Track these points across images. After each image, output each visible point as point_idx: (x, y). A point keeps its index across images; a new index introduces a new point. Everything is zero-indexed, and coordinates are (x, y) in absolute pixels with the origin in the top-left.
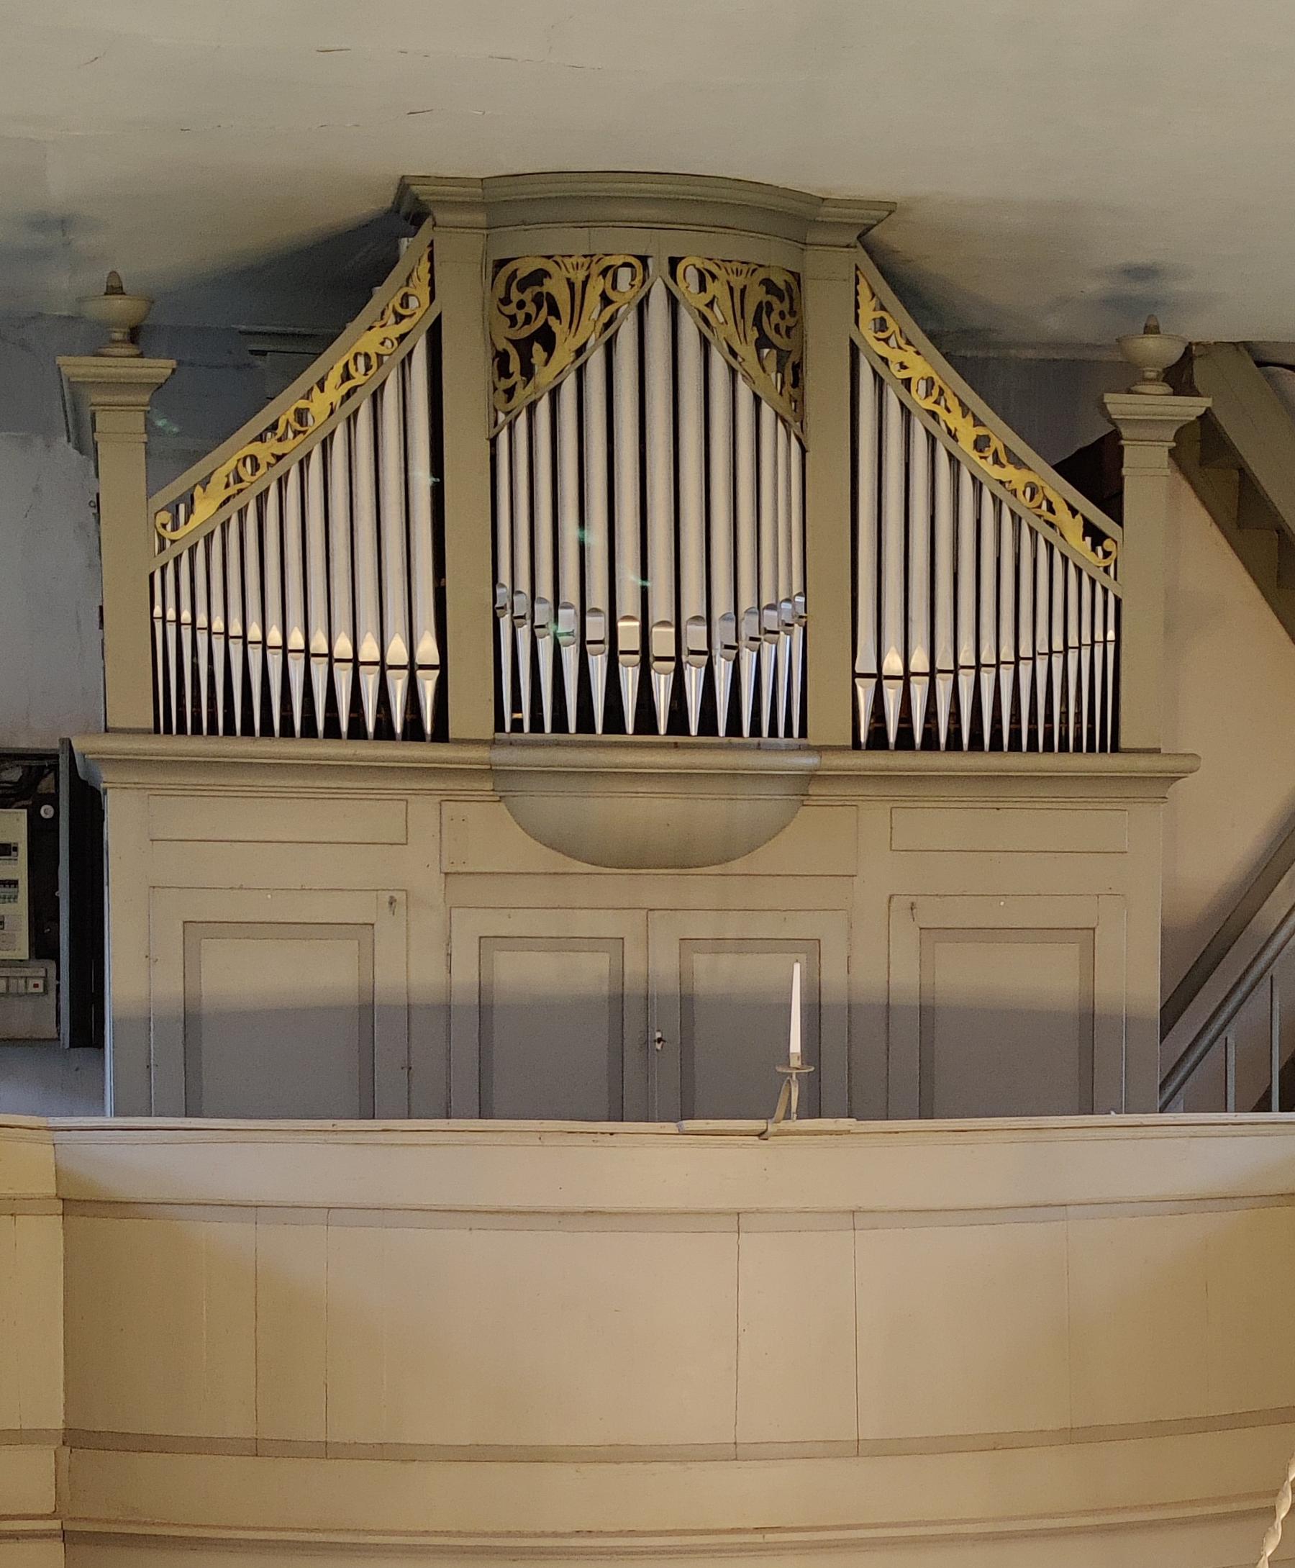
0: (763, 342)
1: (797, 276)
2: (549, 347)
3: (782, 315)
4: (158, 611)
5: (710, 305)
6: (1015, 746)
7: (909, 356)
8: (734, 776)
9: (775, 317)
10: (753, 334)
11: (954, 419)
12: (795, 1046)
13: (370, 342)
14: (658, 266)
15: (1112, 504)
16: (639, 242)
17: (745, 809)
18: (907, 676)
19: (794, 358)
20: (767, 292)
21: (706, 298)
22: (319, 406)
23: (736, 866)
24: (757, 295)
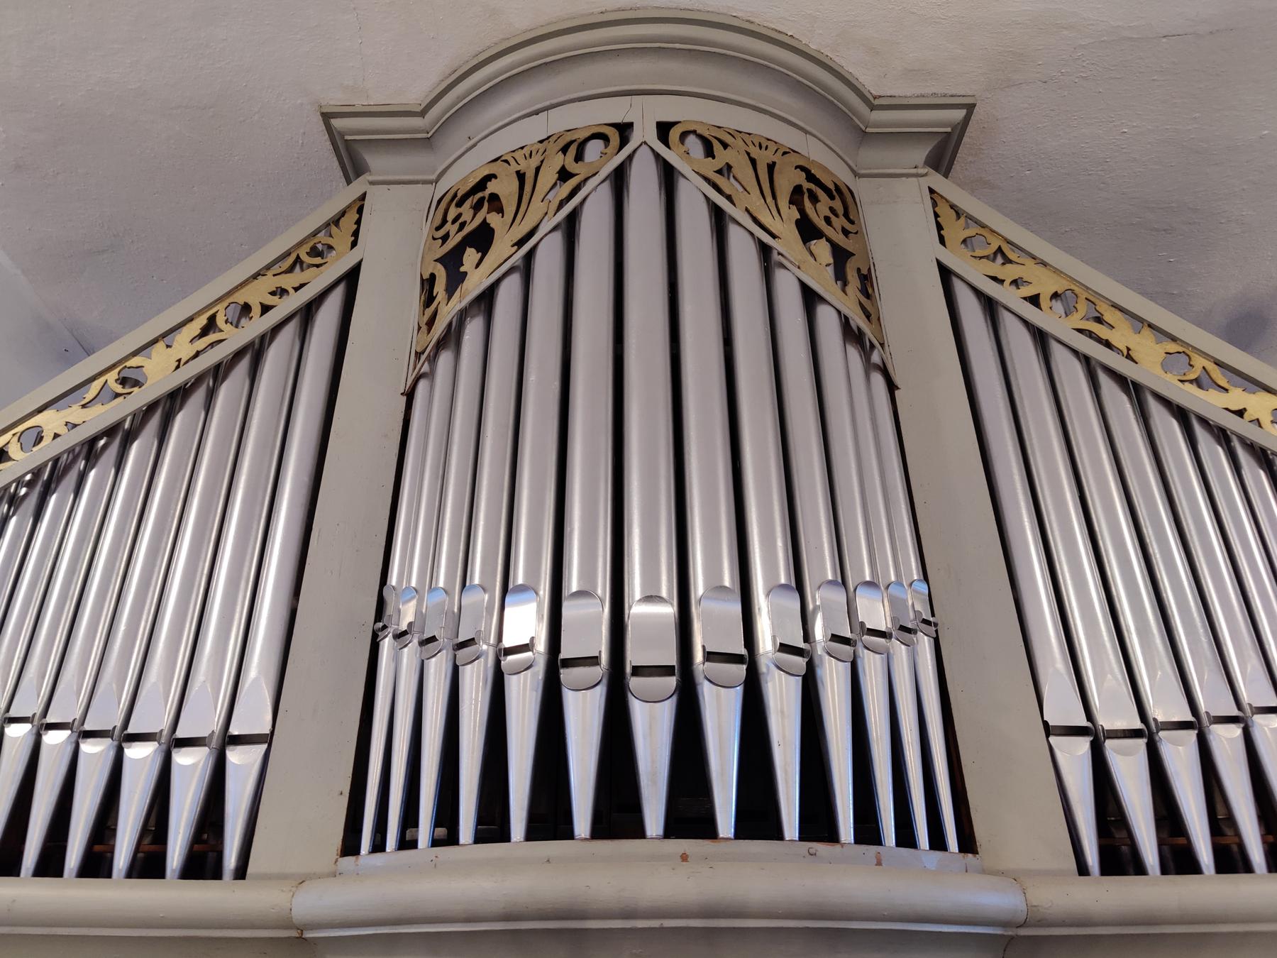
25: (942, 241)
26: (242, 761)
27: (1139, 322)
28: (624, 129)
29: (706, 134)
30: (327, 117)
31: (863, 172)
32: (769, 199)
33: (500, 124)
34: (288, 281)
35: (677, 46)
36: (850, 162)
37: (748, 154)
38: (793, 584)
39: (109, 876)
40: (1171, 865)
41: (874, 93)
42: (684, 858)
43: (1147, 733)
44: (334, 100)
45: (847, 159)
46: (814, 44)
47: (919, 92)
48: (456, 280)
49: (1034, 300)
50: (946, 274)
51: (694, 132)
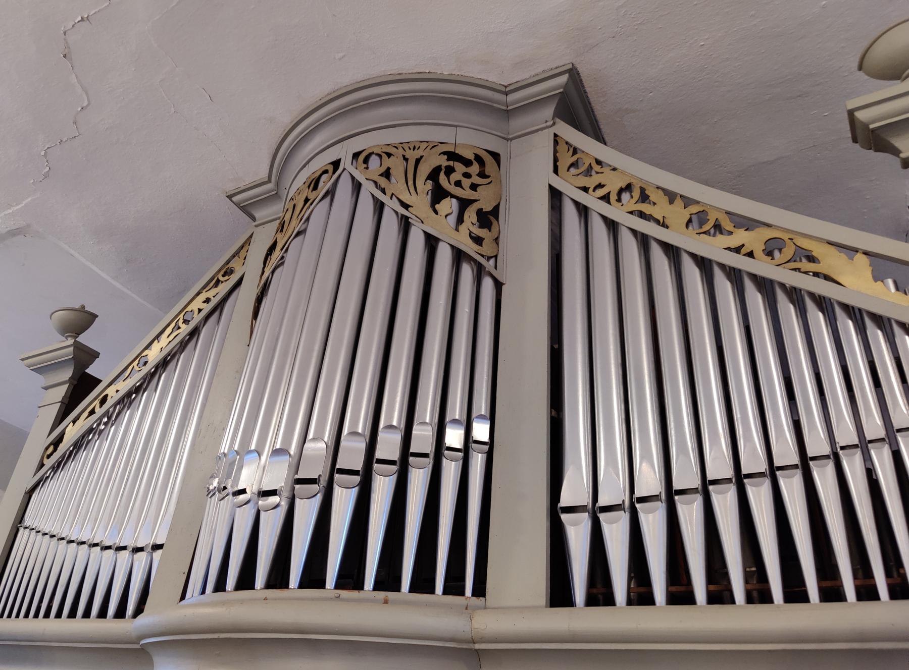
0: (439, 195)
1: (496, 156)
3: (467, 175)
4: (574, 491)
5: (387, 174)
9: (455, 177)
20: (448, 160)
21: (383, 169)
25: (556, 171)
27: (671, 197)
28: (336, 164)
29: (379, 152)
30: (230, 197)
31: (511, 136)
32: (411, 183)
33: (529, 130)
34: (210, 294)
35: (362, 103)
36: (499, 134)
37: (404, 156)
38: (488, 416)
39: (253, 588)
40: (755, 594)
41: (506, 84)
42: (265, 599)
43: (596, 512)
44: (231, 187)
45: (494, 132)
46: (446, 71)
47: (533, 73)
49: (606, 198)
50: (555, 195)
51: (373, 153)
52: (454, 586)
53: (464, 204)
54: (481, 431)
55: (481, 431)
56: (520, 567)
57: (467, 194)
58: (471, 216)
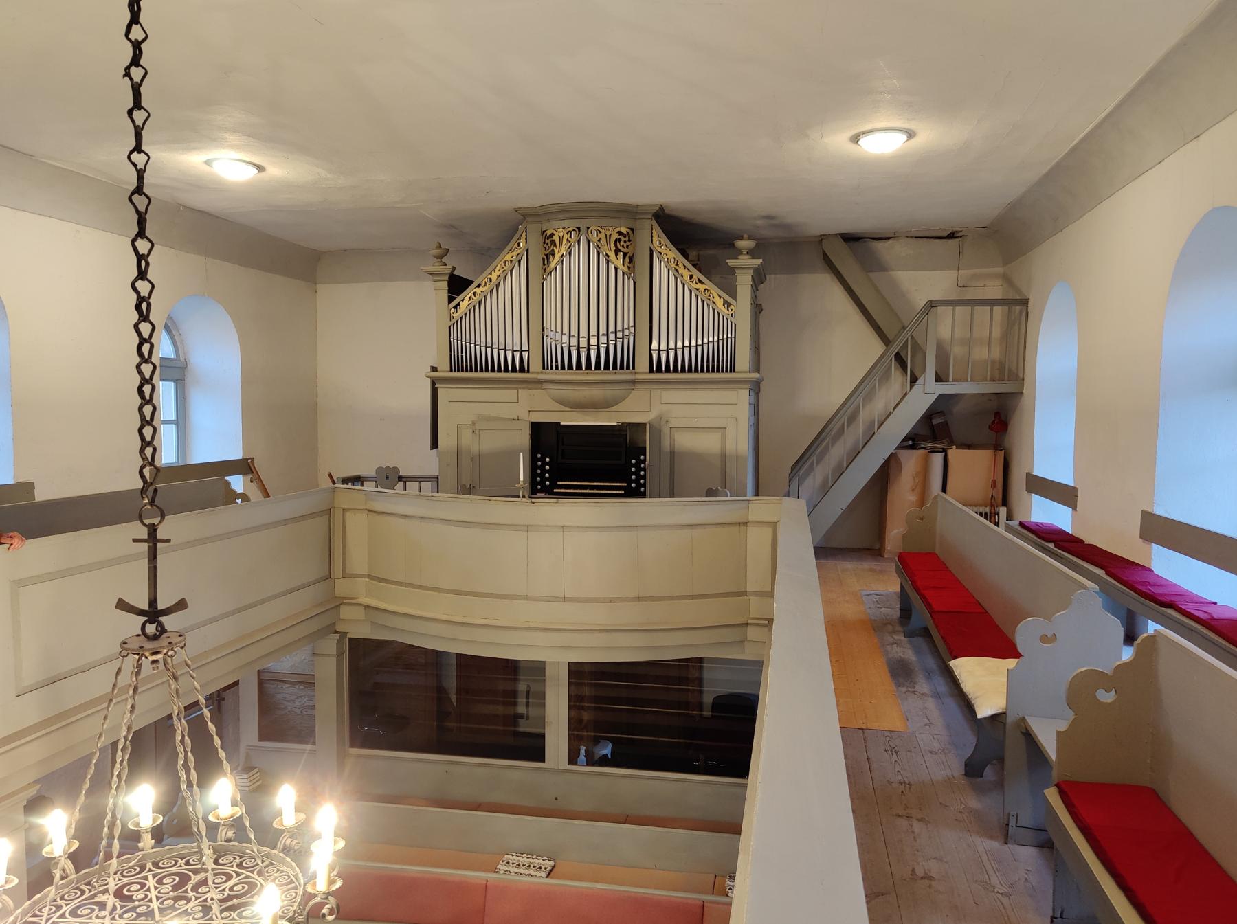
0: (617, 251)
2: (553, 255)
4: (655, 345)
6: (702, 371)
7: (668, 251)
8: (603, 382)
10: (613, 248)
11: (681, 270)
12: (521, 478)
13: (508, 258)
14: (583, 230)
15: (733, 295)
16: (577, 223)
17: (617, 391)
18: (659, 350)
19: (630, 254)
22: (494, 277)
23: (614, 408)
24: (616, 236)
26: (525, 355)
48: (549, 263)
52: (628, 368)
53: (625, 255)
54: (632, 330)
55: (632, 330)
56: (642, 364)
57: (625, 250)
58: (627, 259)
